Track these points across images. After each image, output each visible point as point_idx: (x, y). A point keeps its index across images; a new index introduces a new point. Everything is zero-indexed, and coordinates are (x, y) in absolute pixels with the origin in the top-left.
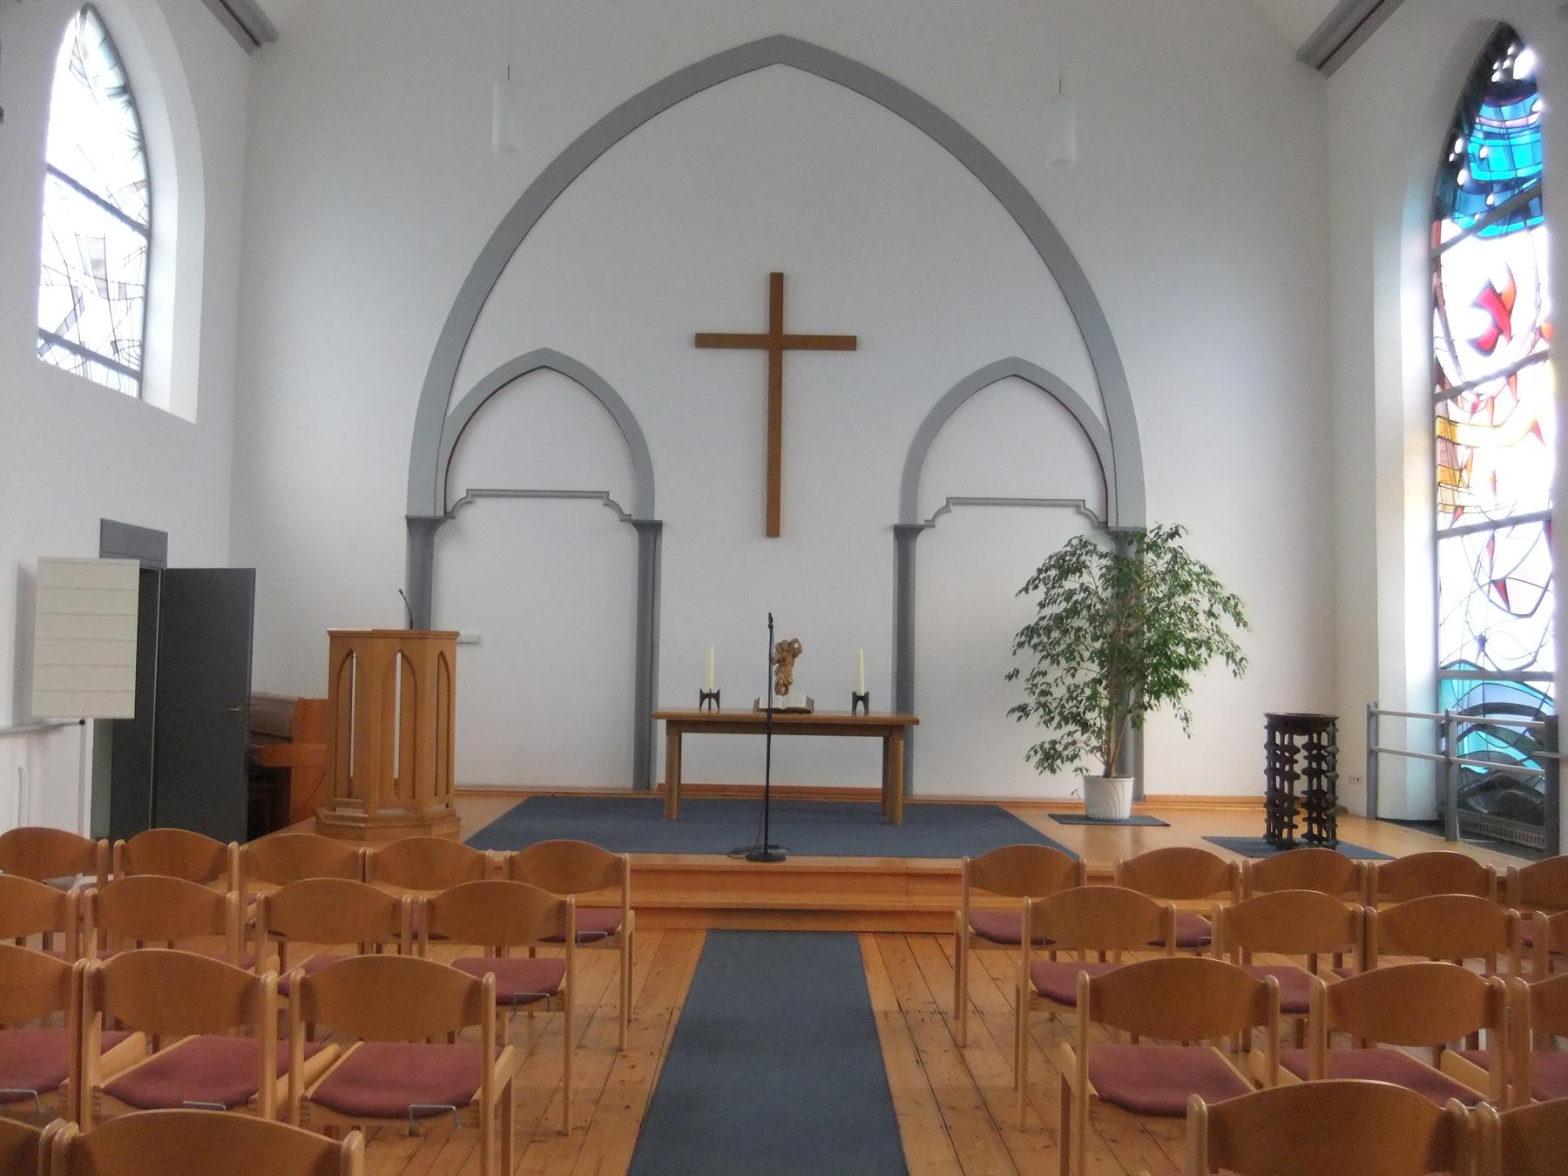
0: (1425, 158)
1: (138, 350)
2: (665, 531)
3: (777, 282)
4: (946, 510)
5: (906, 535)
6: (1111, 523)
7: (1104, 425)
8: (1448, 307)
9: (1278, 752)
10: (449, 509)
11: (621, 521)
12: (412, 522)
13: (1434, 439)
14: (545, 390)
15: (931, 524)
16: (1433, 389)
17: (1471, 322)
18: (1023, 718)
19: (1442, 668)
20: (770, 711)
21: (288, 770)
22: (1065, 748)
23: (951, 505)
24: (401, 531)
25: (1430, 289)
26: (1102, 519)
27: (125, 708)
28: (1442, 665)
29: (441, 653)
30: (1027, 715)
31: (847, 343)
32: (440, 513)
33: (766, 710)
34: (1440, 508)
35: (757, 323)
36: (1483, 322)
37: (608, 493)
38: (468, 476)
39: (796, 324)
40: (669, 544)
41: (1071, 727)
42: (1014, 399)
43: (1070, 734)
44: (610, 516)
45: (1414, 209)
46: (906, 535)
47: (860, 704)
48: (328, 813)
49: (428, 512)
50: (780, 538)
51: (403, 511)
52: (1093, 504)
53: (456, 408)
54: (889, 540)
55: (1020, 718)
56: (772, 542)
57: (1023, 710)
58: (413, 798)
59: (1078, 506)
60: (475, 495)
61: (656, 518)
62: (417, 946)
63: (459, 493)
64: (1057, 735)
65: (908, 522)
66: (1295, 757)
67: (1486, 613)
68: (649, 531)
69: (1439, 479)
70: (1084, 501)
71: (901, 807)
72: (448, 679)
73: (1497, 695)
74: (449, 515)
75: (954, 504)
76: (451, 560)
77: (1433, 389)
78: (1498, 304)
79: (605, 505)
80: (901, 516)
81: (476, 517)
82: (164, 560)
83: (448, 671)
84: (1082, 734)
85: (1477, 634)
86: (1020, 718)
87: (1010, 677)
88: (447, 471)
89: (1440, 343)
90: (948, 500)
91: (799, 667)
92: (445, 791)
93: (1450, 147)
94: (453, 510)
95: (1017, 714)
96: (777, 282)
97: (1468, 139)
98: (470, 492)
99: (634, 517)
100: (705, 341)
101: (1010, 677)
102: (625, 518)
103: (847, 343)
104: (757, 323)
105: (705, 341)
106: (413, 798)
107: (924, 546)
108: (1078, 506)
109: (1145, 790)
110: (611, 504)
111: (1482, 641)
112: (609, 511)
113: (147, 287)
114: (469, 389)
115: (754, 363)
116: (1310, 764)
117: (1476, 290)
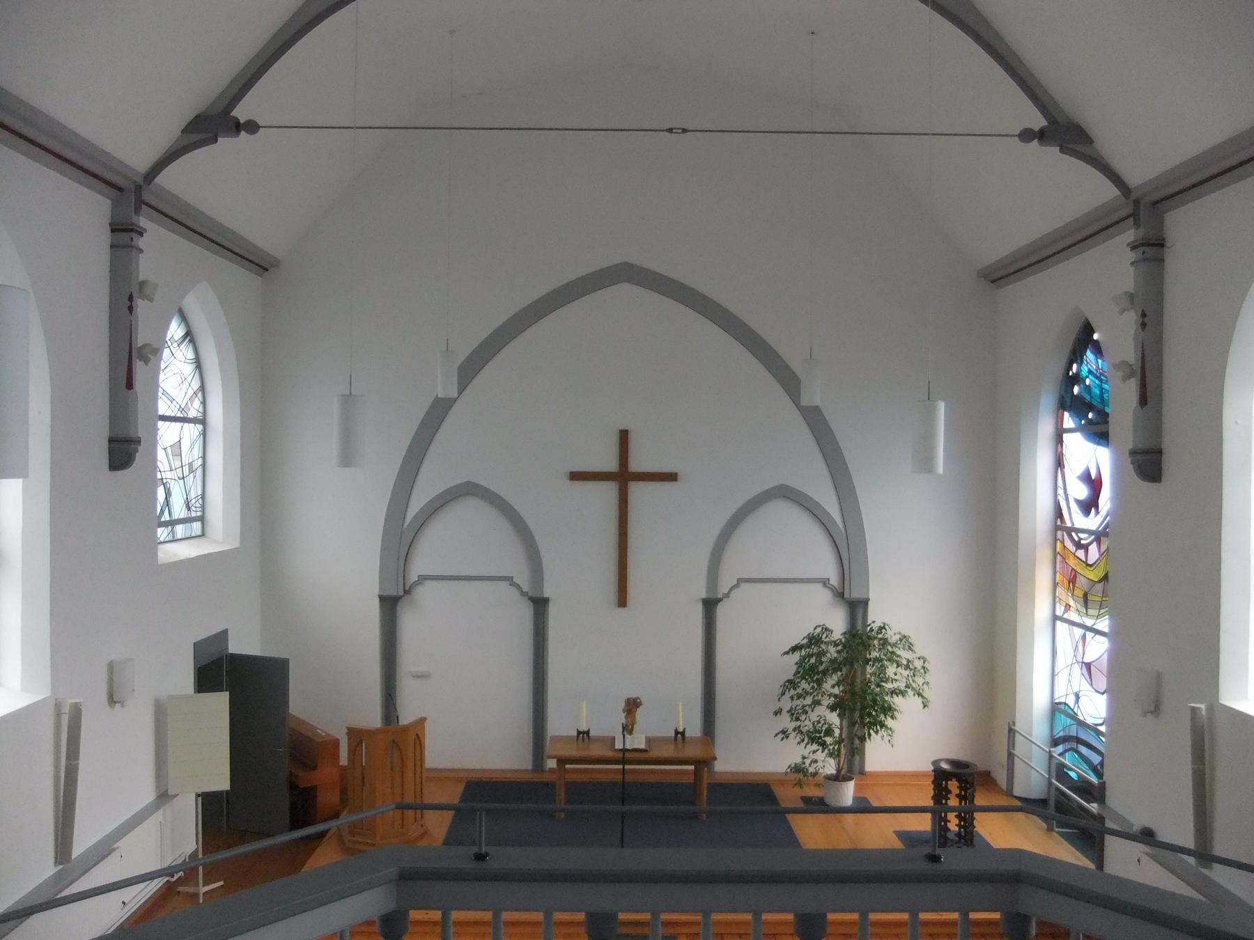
0: (1056, 368)
1: (200, 501)
2: (551, 604)
3: (624, 436)
4: (737, 586)
5: (710, 605)
6: (846, 596)
7: (845, 534)
8: (1067, 469)
9: (944, 793)
10: (407, 589)
11: (521, 595)
12: (383, 599)
13: (1055, 554)
14: (469, 508)
15: (727, 595)
16: (1056, 522)
17: (1081, 491)
18: (785, 739)
19: (1056, 703)
20: (624, 750)
21: (315, 787)
22: (810, 765)
23: (740, 583)
24: (377, 602)
25: (1056, 455)
26: (841, 591)
27: (222, 783)
28: (1057, 701)
29: (417, 735)
30: (787, 737)
31: (671, 477)
32: (401, 593)
33: (621, 750)
34: (1057, 600)
35: (611, 465)
36: (1082, 492)
37: (512, 577)
38: (420, 565)
39: (636, 465)
40: (553, 611)
41: (815, 747)
42: (781, 511)
43: (814, 752)
44: (514, 592)
45: (1048, 401)
46: (710, 605)
47: (679, 736)
48: (350, 838)
49: (392, 592)
50: (626, 608)
51: (377, 591)
52: (834, 581)
53: (411, 522)
54: (699, 609)
55: (782, 739)
56: (621, 610)
57: (785, 734)
58: (402, 828)
59: (825, 583)
60: (423, 579)
61: (545, 596)
62: (341, 763)
63: (413, 578)
64: (806, 753)
65: (712, 596)
66: (949, 796)
67: (1079, 681)
68: (540, 605)
69: (1058, 580)
70: (829, 579)
71: (706, 786)
72: (421, 753)
73: (1083, 735)
74: (407, 592)
75: (742, 582)
76: (410, 623)
77: (1056, 522)
78: (1095, 485)
79: (510, 585)
80: (707, 592)
81: (425, 593)
82: (227, 649)
83: (420, 744)
84: (822, 752)
85: (1075, 691)
86: (782, 739)
87: (776, 713)
88: (405, 560)
89: (1060, 491)
90: (738, 579)
91: (640, 713)
92: (420, 816)
93: (1070, 368)
94: (410, 589)
95: (781, 736)
96: (624, 436)
97: (1080, 365)
98: (421, 577)
99: (530, 594)
100: (576, 476)
101: (776, 713)
102: (523, 594)
103: (671, 477)
104: (611, 465)
105: (576, 476)
106: (402, 828)
107: (722, 611)
108: (825, 583)
109: (866, 767)
110: (513, 584)
111: (1077, 697)
112: (514, 590)
113: (204, 458)
114: (418, 510)
115: (608, 491)
116: (960, 792)
117: (1080, 470)
